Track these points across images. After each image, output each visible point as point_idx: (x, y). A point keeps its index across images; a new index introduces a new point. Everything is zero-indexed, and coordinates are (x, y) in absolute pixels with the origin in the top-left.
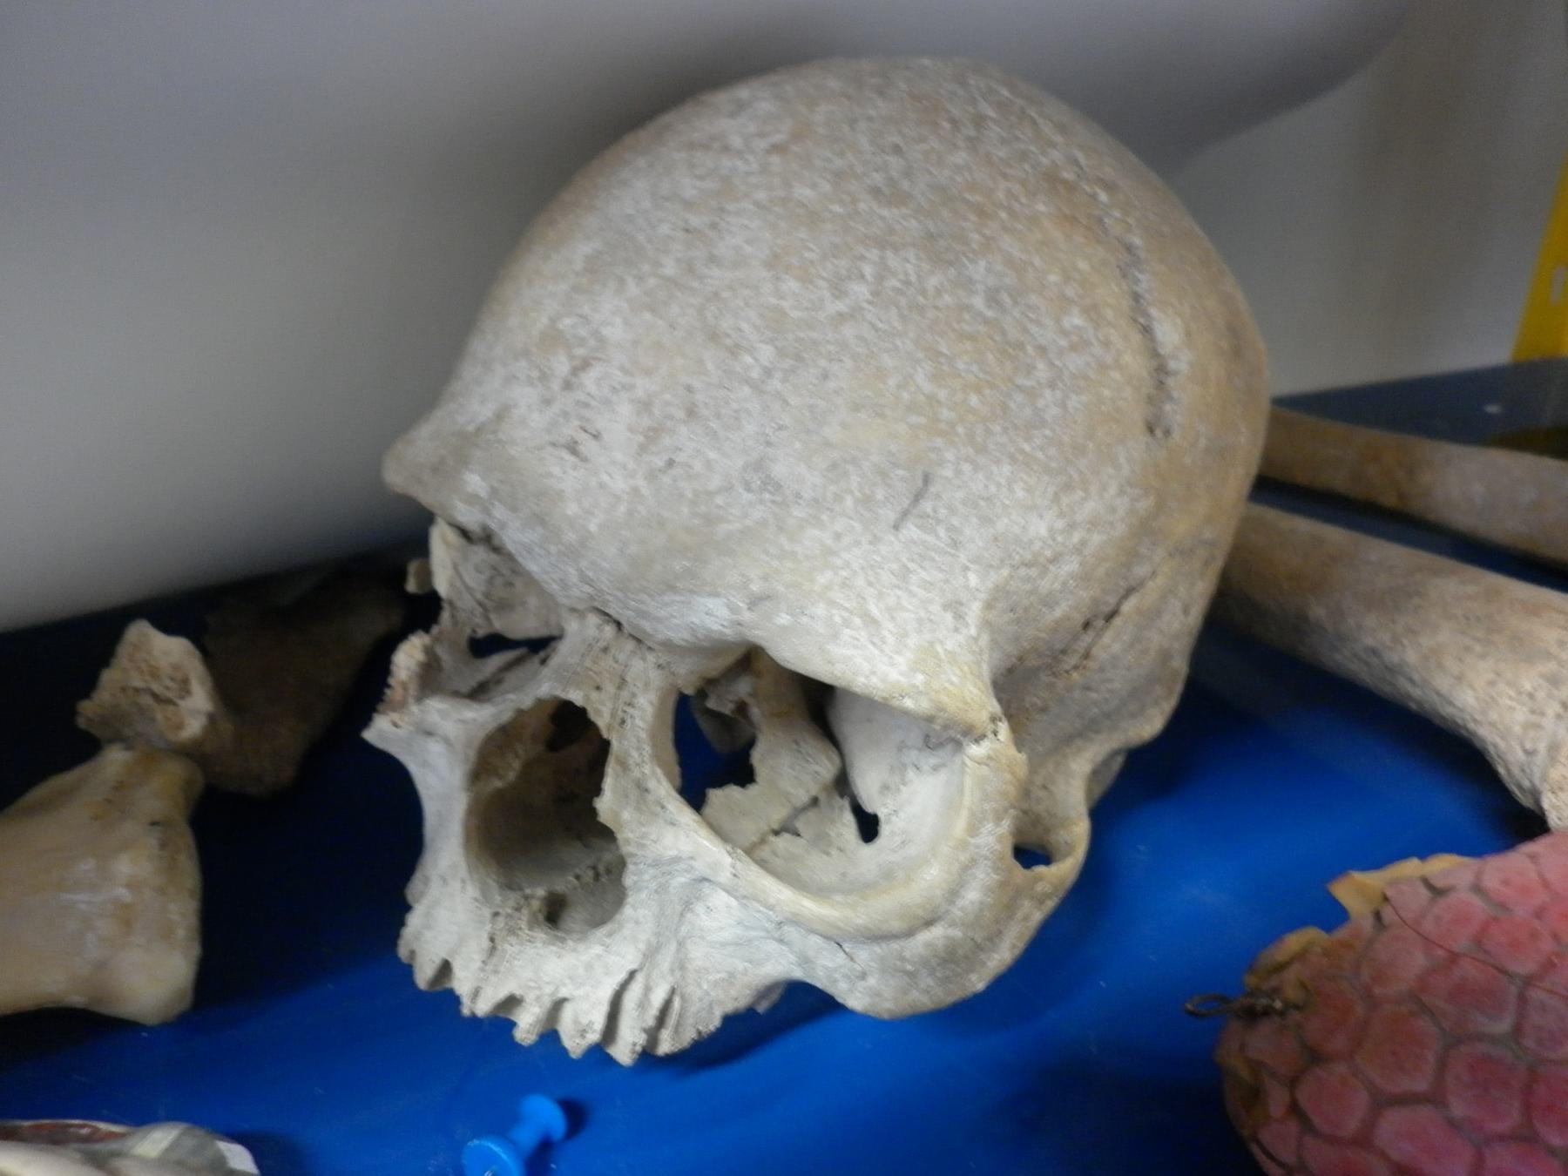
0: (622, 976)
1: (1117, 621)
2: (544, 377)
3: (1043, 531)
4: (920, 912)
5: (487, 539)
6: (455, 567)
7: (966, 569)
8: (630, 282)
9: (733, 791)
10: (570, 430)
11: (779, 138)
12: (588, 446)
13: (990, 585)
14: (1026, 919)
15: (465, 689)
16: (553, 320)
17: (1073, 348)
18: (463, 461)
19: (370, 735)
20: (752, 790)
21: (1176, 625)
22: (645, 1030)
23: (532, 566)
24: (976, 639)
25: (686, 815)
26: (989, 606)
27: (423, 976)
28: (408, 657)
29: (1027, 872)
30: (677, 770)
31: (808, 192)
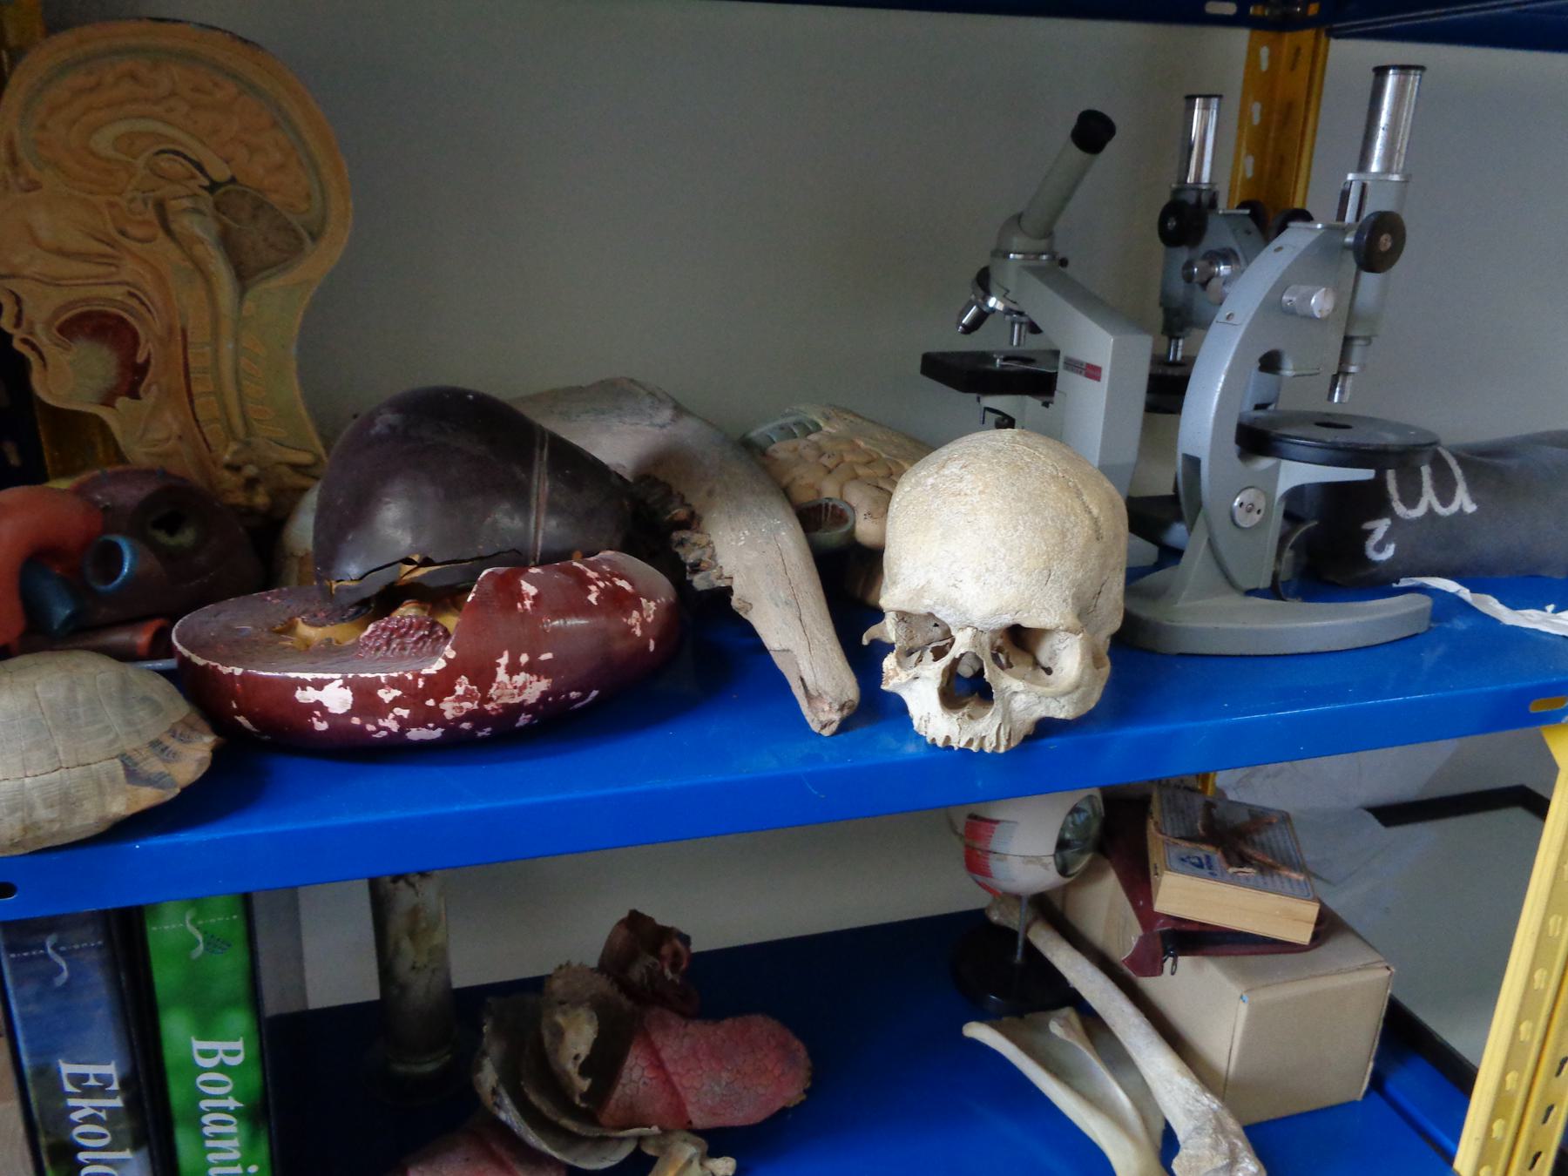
19: (884, 687)
27: (940, 743)
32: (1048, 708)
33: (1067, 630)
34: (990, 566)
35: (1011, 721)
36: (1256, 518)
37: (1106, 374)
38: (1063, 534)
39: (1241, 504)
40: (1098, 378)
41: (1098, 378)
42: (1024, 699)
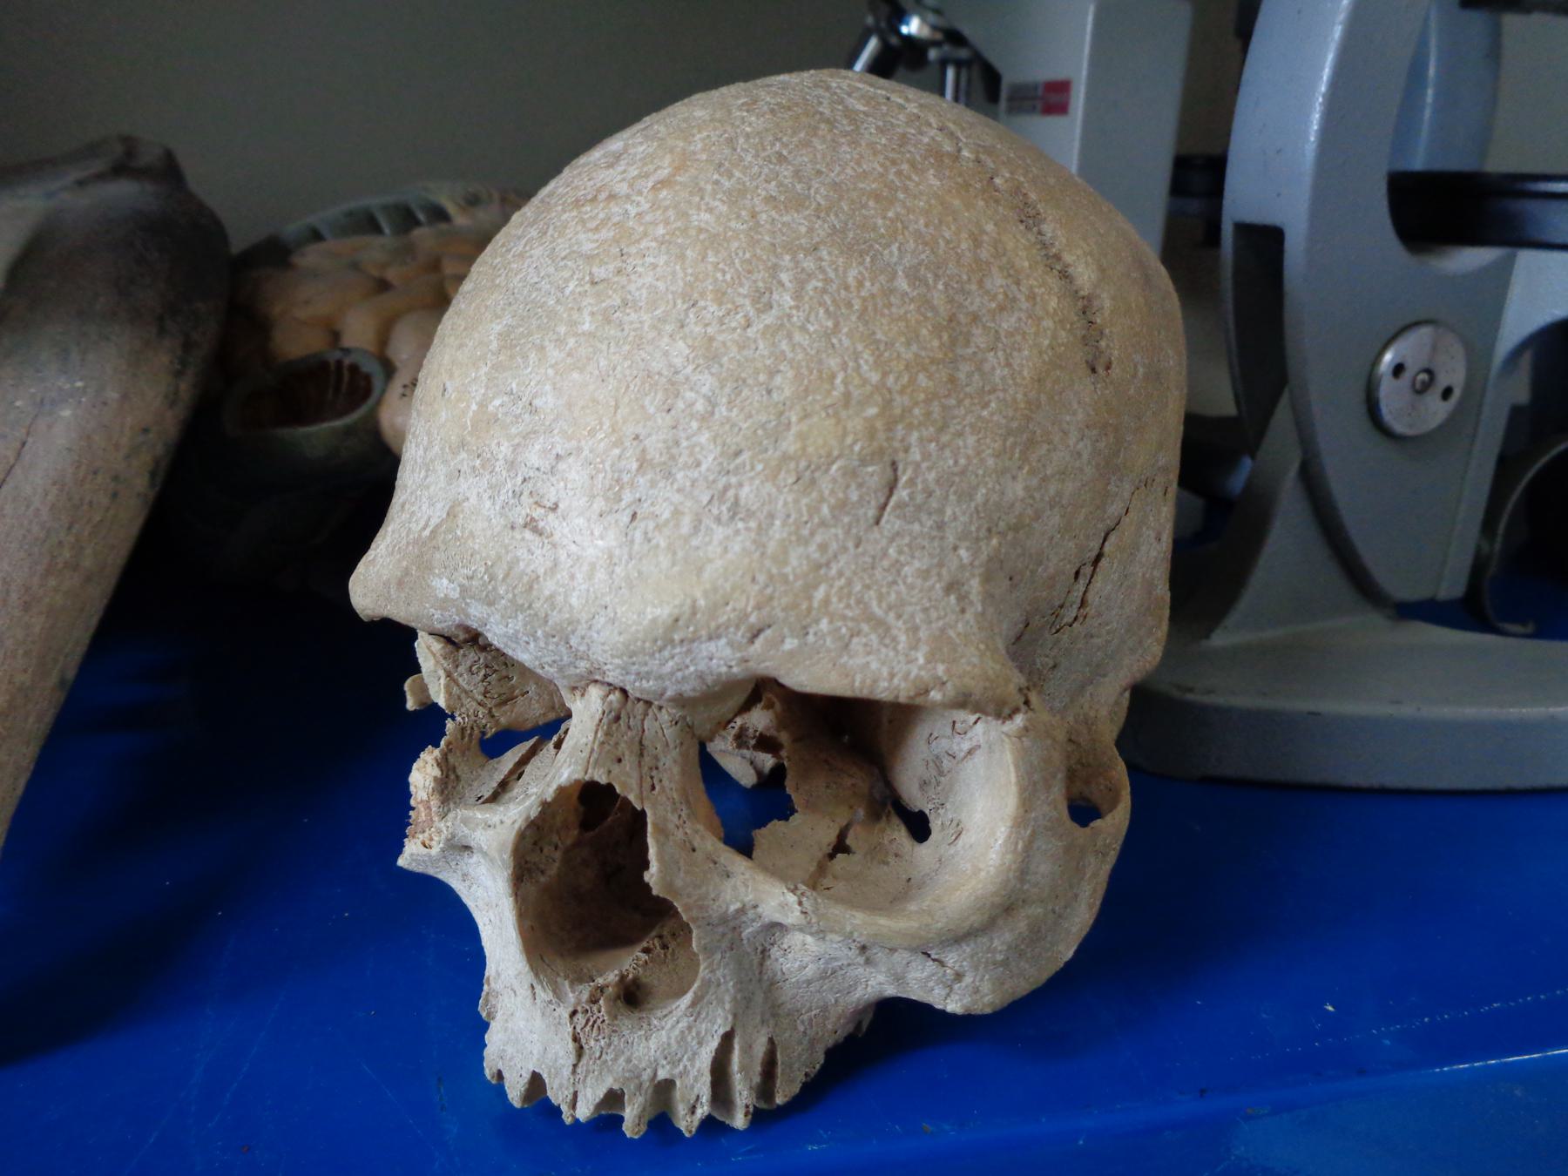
0: (714, 1044)
1: (1104, 562)
2: (488, 464)
3: (1021, 493)
4: (997, 900)
5: (474, 639)
6: (449, 675)
7: (955, 548)
8: (550, 347)
9: (776, 825)
10: (520, 514)
11: (664, 173)
12: (551, 522)
13: (984, 557)
14: (1095, 875)
15: (487, 795)
16: (482, 405)
17: (1002, 308)
18: (426, 567)
19: (401, 862)
20: (796, 819)
21: (1154, 554)
22: (275, 253)
23: (524, 656)
24: (983, 614)
25: (738, 863)
26: (987, 579)
27: (515, 1093)
28: (423, 775)
29: (1087, 830)
30: (717, 821)
31: (705, 216)
32: (899, 979)
33: (963, 702)
34: (654, 446)
35: (774, 1011)
36: (1436, 411)
37: (1079, 99)
38: (954, 329)
39: (1398, 370)
40: (1060, 108)
41: (1060, 108)
42: (815, 939)
